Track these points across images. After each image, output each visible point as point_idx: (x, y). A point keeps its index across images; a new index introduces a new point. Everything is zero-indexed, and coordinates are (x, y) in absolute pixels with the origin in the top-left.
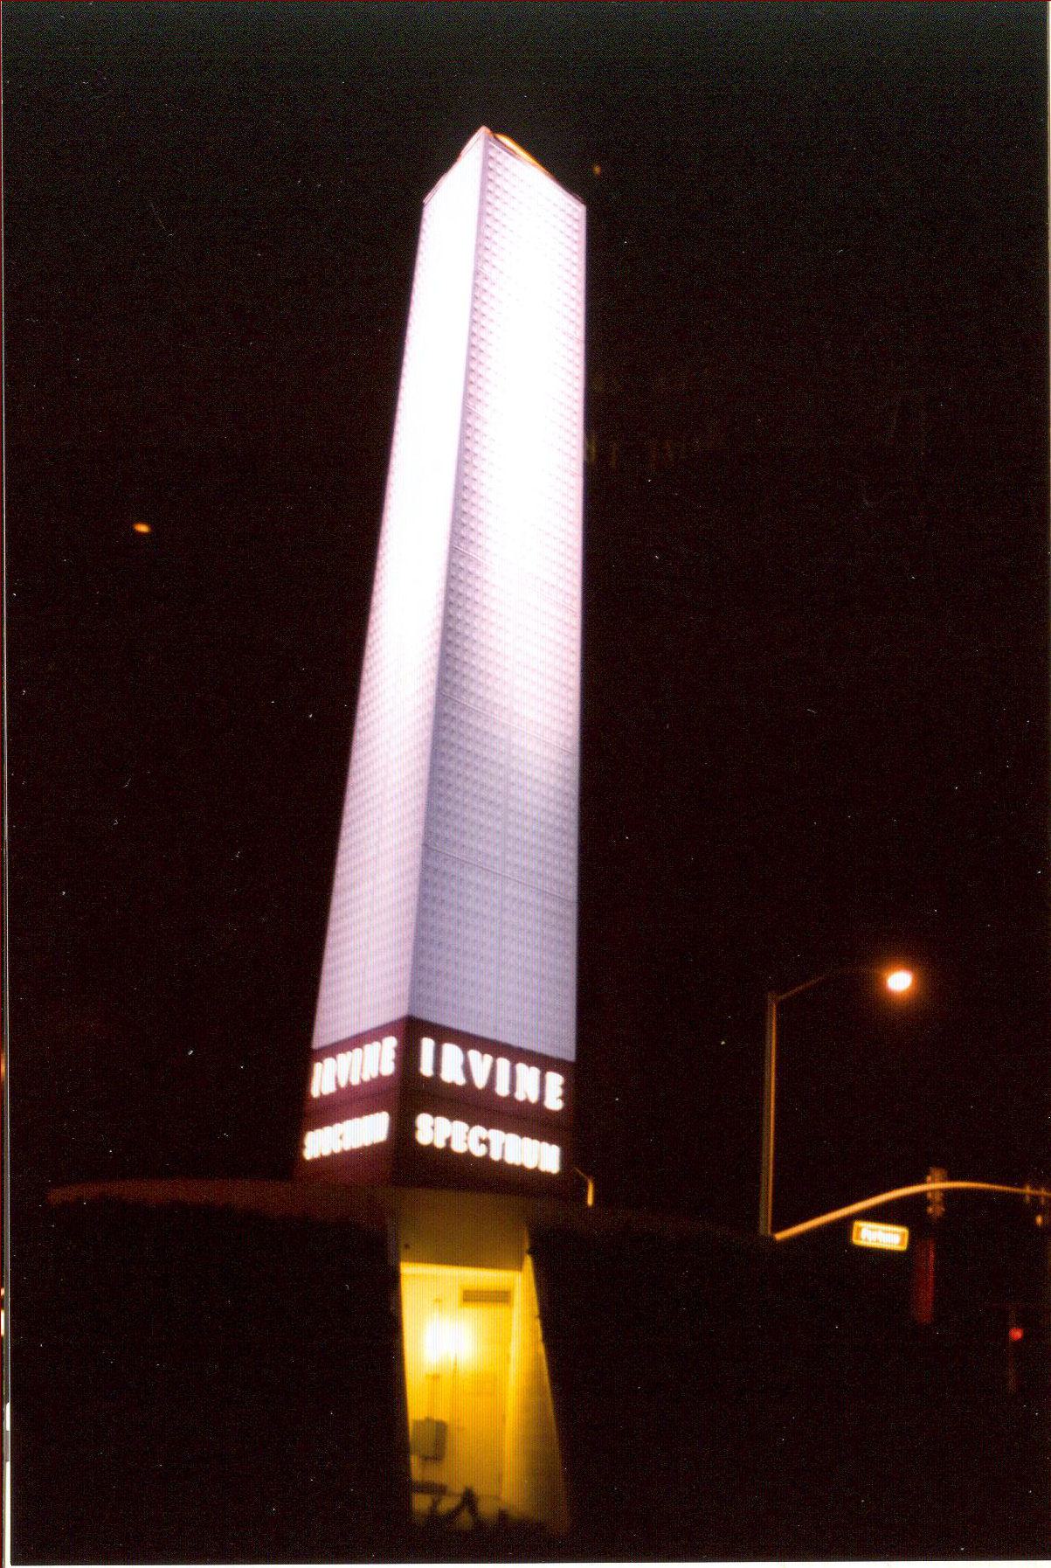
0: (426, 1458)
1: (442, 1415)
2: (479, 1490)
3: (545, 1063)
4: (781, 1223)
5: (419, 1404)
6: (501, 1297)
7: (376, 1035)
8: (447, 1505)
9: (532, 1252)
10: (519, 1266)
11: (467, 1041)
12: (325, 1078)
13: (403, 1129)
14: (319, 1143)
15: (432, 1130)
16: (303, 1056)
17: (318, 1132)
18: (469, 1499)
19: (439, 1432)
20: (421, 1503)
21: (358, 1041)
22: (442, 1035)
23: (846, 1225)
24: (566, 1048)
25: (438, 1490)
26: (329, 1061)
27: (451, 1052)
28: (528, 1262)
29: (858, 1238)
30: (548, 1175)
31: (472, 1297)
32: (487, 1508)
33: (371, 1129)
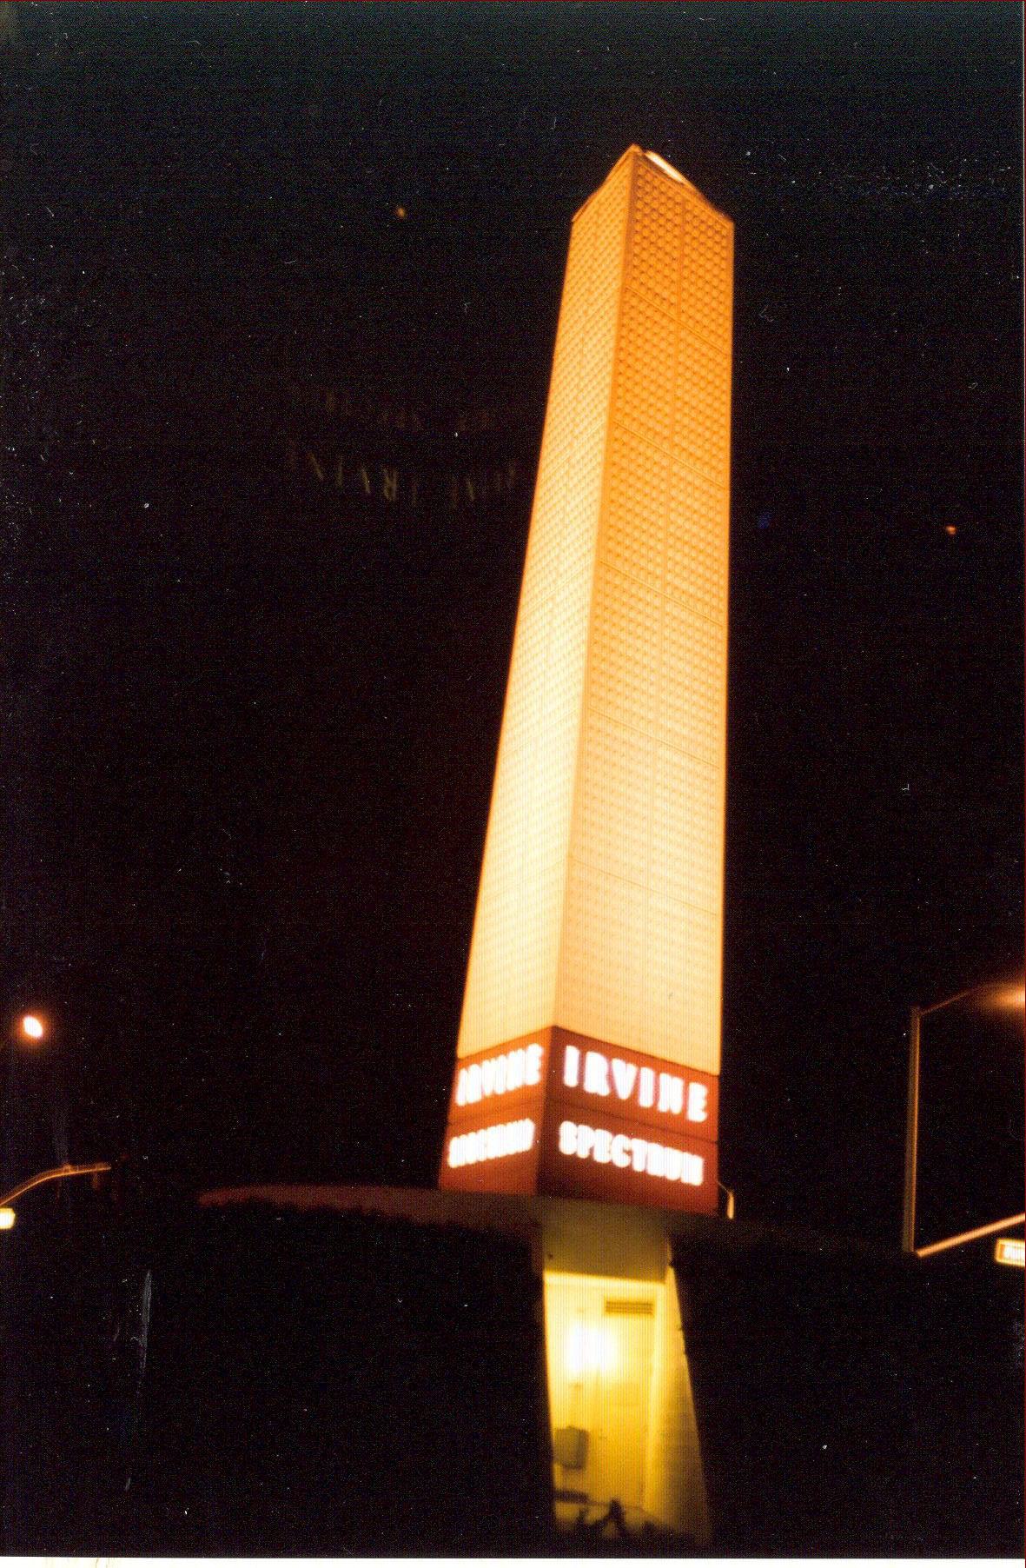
0: (567, 1467)
1: (585, 1424)
2: (627, 1500)
3: (688, 1074)
4: (921, 1242)
5: (563, 1410)
6: (645, 1308)
7: (522, 1042)
8: (596, 1514)
9: (676, 1264)
10: (661, 1278)
11: (611, 1051)
12: (470, 1087)
13: (547, 1137)
14: (464, 1151)
15: (576, 1139)
16: (445, 1066)
17: (463, 1137)
18: (616, 1510)
19: (581, 1439)
20: (565, 1511)
21: (503, 1049)
22: (586, 1044)
23: (989, 1242)
24: (712, 1062)
25: (581, 1498)
26: (474, 1068)
27: (595, 1060)
28: (671, 1274)
29: (1001, 1256)
30: (689, 1188)
31: (613, 1307)
32: (632, 1518)
33: (516, 1138)
